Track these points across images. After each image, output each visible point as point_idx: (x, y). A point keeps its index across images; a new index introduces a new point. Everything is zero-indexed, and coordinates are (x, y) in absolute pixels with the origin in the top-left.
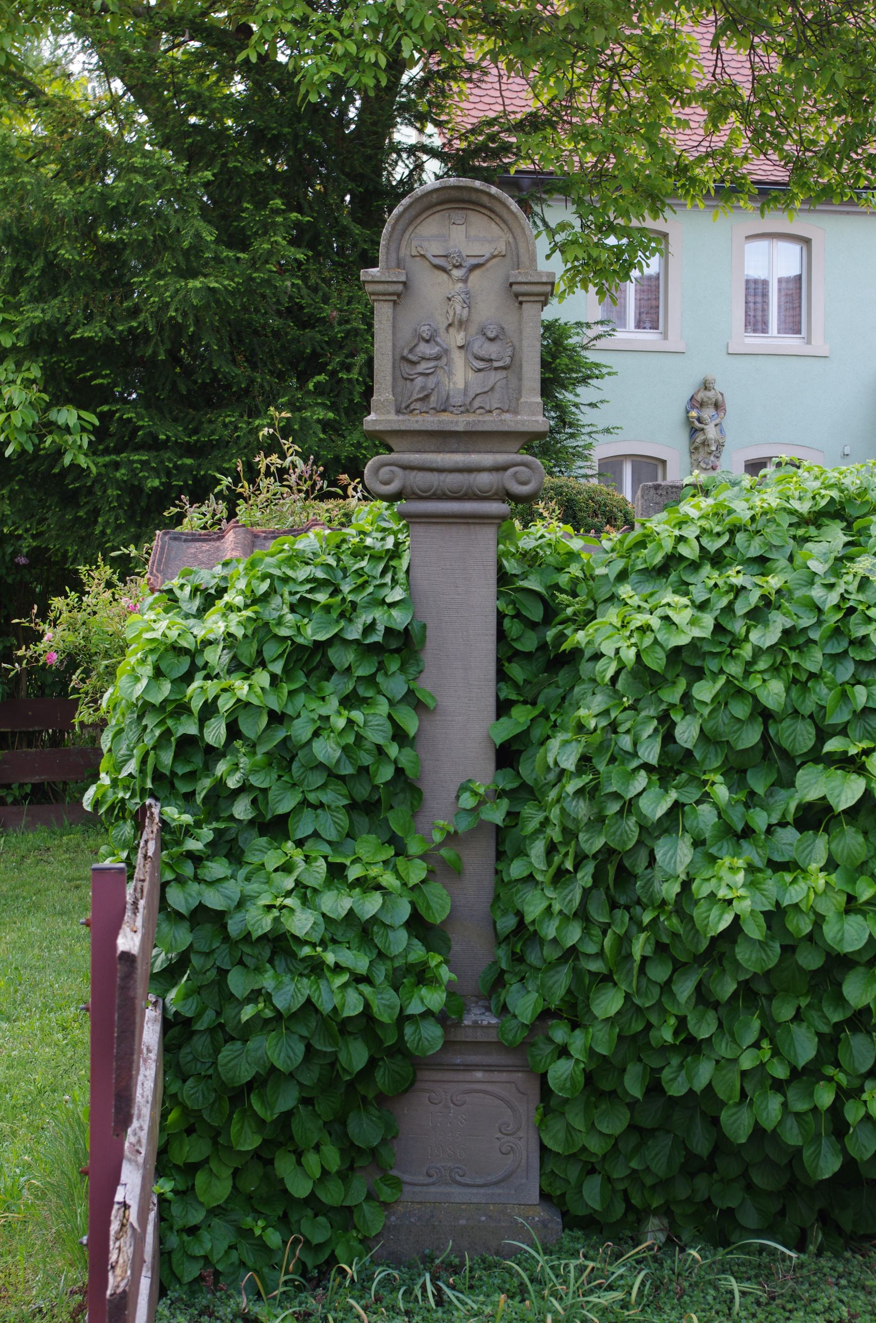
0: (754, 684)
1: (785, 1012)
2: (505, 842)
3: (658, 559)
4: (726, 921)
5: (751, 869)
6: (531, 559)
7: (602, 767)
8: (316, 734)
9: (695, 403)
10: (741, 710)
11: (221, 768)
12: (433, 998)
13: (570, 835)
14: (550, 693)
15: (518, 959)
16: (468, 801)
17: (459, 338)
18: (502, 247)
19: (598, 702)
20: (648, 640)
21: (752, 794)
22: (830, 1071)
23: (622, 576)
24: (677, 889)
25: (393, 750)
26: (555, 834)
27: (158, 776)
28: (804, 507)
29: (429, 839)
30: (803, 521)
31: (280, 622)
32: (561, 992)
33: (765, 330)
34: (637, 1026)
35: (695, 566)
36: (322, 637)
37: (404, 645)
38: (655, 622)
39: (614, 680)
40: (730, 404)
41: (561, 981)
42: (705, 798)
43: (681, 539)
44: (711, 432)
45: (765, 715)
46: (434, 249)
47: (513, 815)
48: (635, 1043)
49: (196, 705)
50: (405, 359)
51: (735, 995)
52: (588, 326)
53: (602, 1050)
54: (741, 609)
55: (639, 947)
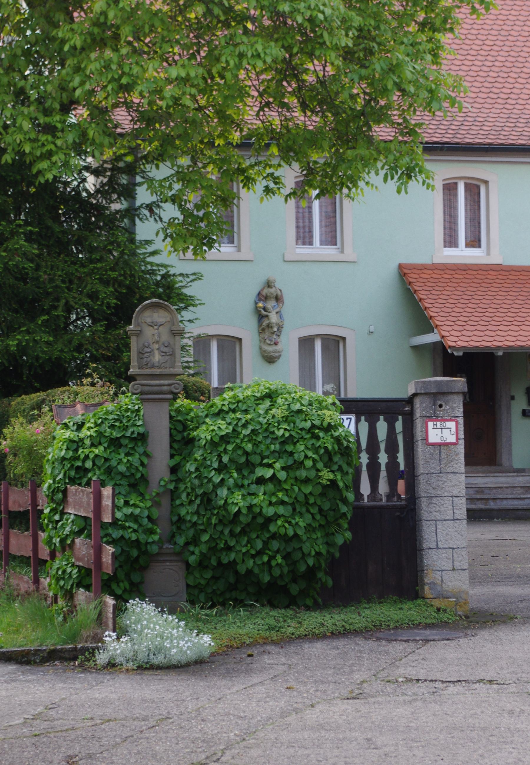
0: (244, 445)
1: (254, 536)
2: (173, 494)
3: (217, 411)
4: (237, 509)
5: (243, 495)
6: (178, 411)
7: (202, 470)
8: (118, 464)
9: (261, 297)
10: (240, 452)
11: (90, 475)
12: (156, 538)
13: (193, 489)
14: (186, 452)
15: (179, 528)
16: (162, 483)
17: (157, 346)
18: (169, 319)
19: (201, 452)
20: (214, 434)
21: (244, 475)
22: (267, 551)
23: (207, 416)
24: (223, 502)
25: (141, 468)
26: (189, 490)
27: (70, 479)
28: (258, 395)
29: (151, 495)
30: (259, 399)
31: (105, 431)
32: (191, 535)
33: (311, 243)
34: (214, 545)
35: (227, 413)
36: (119, 436)
37: (142, 438)
38: (216, 428)
39: (205, 445)
40: (286, 298)
41: (191, 533)
42: (231, 477)
43: (223, 405)
44: (274, 318)
45: (246, 453)
46: (149, 320)
47: (176, 488)
48: (213, 549)
49: (82, 456)
50: (140, 353)
51: (240, 532)
52: (187, 276)
53: (204, 551)
54: (240, 424)
55: (214, 521)
